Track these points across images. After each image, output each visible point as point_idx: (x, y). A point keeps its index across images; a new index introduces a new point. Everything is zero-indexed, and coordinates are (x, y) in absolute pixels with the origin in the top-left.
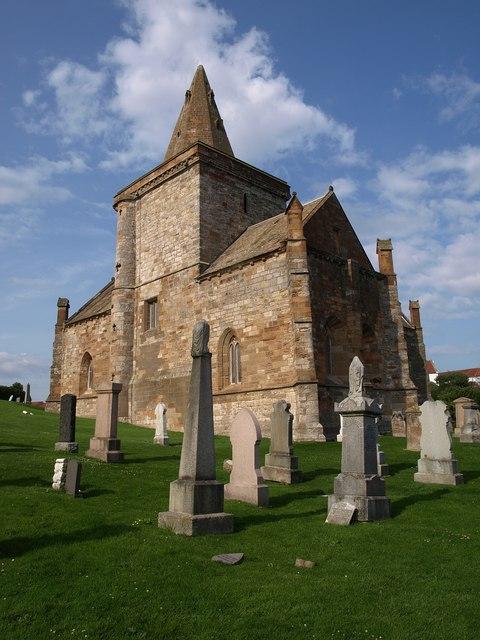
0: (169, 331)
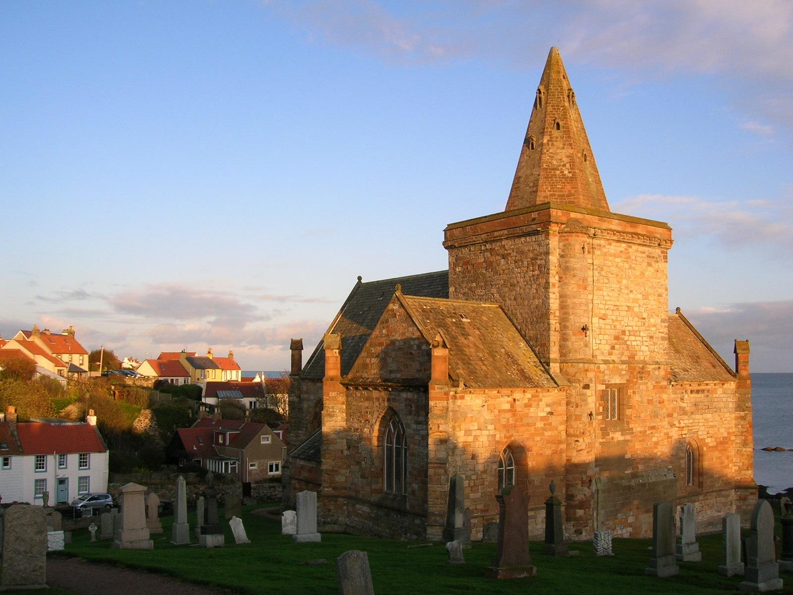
0: (639, 429)
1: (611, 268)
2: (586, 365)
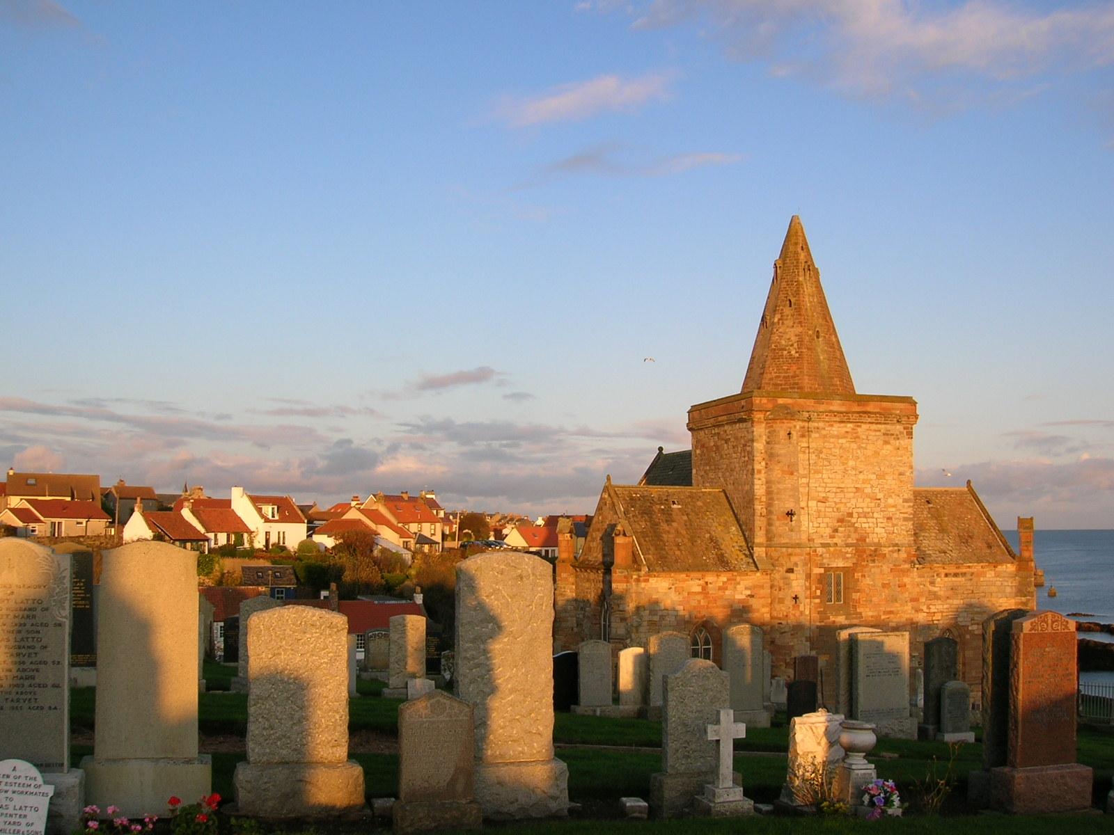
1: (833, 450)
2: (790, 550)
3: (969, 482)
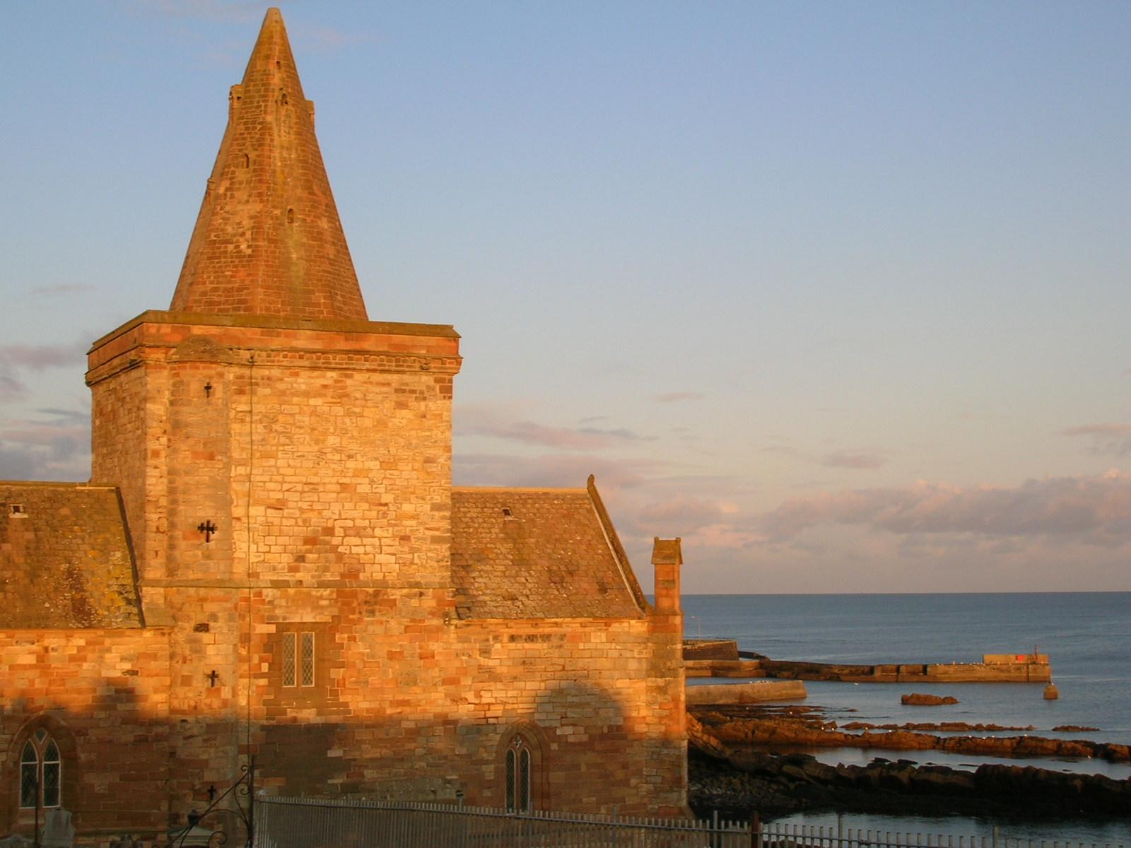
1: (297, 417)
2: (202, 592)
3: (591, 479)
